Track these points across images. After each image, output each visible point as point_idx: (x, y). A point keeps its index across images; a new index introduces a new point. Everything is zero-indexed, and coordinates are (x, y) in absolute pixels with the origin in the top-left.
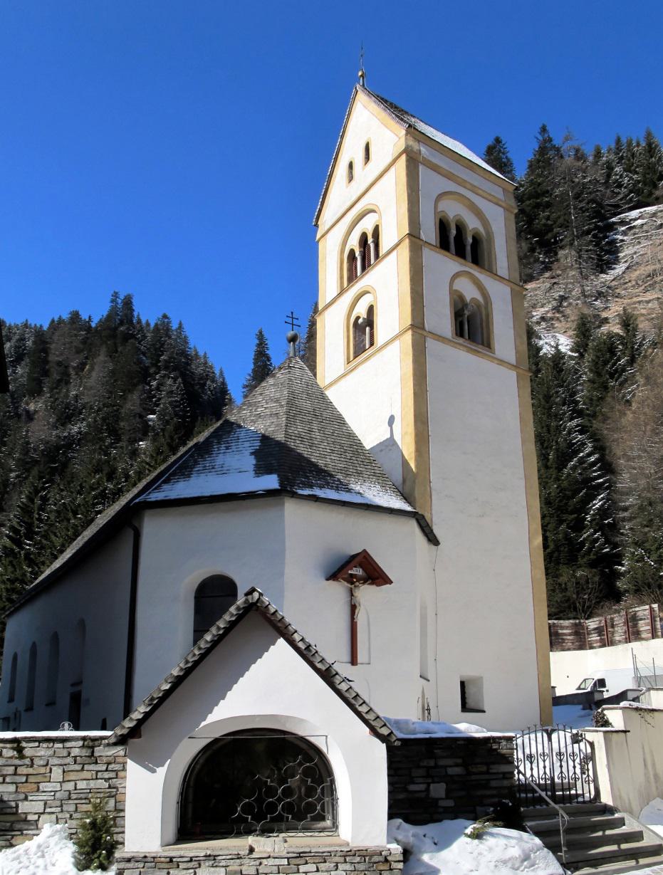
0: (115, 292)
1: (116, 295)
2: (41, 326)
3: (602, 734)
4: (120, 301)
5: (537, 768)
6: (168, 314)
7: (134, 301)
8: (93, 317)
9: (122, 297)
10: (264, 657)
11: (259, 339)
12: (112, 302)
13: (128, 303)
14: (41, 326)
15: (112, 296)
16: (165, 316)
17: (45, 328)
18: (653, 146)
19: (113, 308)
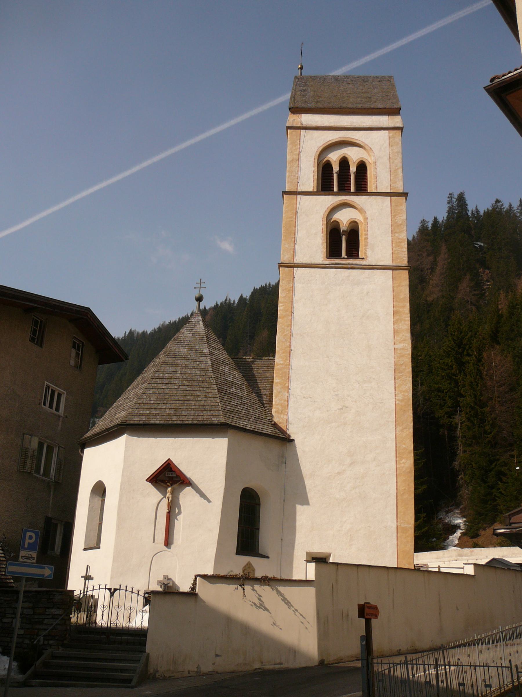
0: (450, 194)
1: (451, 196)
2: (488, 209)
3: (9, 566)
4: (454, 200)
5: (392, 125)
6: (499, 199)
7: (466, 196)
8: (177, 521)
9: (456, 197)
10: (157, 439)
11: (193, 585)
12: (448, 203)
13: (461, 198)
14: (488, 209)
15: (448, 198)
16: (497, 201)
17: (148, 332)
18: (437, 223)
19: (450, 208)
